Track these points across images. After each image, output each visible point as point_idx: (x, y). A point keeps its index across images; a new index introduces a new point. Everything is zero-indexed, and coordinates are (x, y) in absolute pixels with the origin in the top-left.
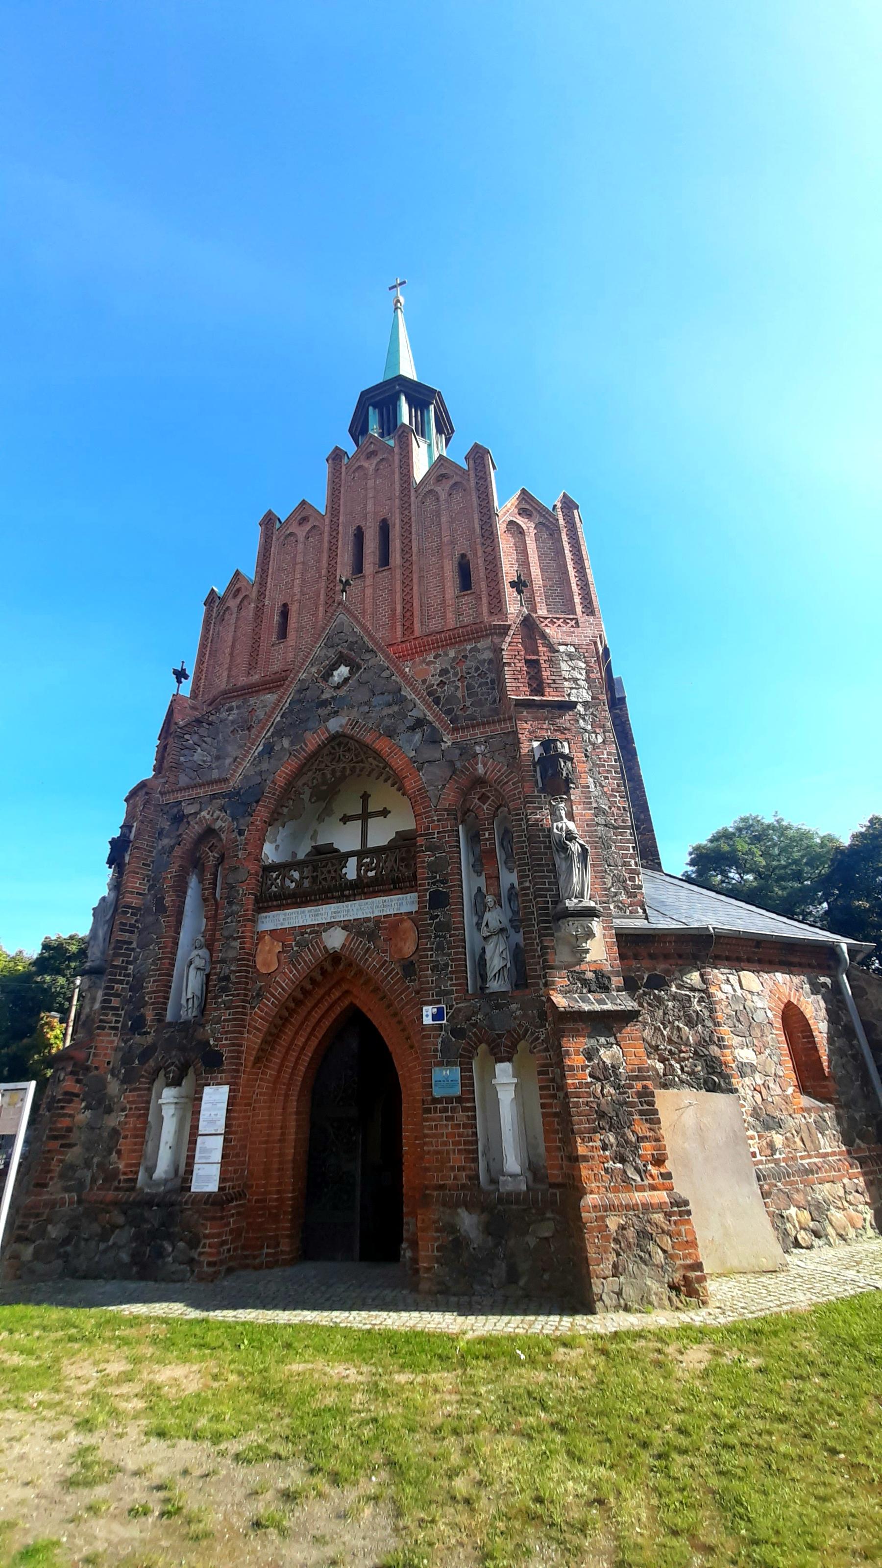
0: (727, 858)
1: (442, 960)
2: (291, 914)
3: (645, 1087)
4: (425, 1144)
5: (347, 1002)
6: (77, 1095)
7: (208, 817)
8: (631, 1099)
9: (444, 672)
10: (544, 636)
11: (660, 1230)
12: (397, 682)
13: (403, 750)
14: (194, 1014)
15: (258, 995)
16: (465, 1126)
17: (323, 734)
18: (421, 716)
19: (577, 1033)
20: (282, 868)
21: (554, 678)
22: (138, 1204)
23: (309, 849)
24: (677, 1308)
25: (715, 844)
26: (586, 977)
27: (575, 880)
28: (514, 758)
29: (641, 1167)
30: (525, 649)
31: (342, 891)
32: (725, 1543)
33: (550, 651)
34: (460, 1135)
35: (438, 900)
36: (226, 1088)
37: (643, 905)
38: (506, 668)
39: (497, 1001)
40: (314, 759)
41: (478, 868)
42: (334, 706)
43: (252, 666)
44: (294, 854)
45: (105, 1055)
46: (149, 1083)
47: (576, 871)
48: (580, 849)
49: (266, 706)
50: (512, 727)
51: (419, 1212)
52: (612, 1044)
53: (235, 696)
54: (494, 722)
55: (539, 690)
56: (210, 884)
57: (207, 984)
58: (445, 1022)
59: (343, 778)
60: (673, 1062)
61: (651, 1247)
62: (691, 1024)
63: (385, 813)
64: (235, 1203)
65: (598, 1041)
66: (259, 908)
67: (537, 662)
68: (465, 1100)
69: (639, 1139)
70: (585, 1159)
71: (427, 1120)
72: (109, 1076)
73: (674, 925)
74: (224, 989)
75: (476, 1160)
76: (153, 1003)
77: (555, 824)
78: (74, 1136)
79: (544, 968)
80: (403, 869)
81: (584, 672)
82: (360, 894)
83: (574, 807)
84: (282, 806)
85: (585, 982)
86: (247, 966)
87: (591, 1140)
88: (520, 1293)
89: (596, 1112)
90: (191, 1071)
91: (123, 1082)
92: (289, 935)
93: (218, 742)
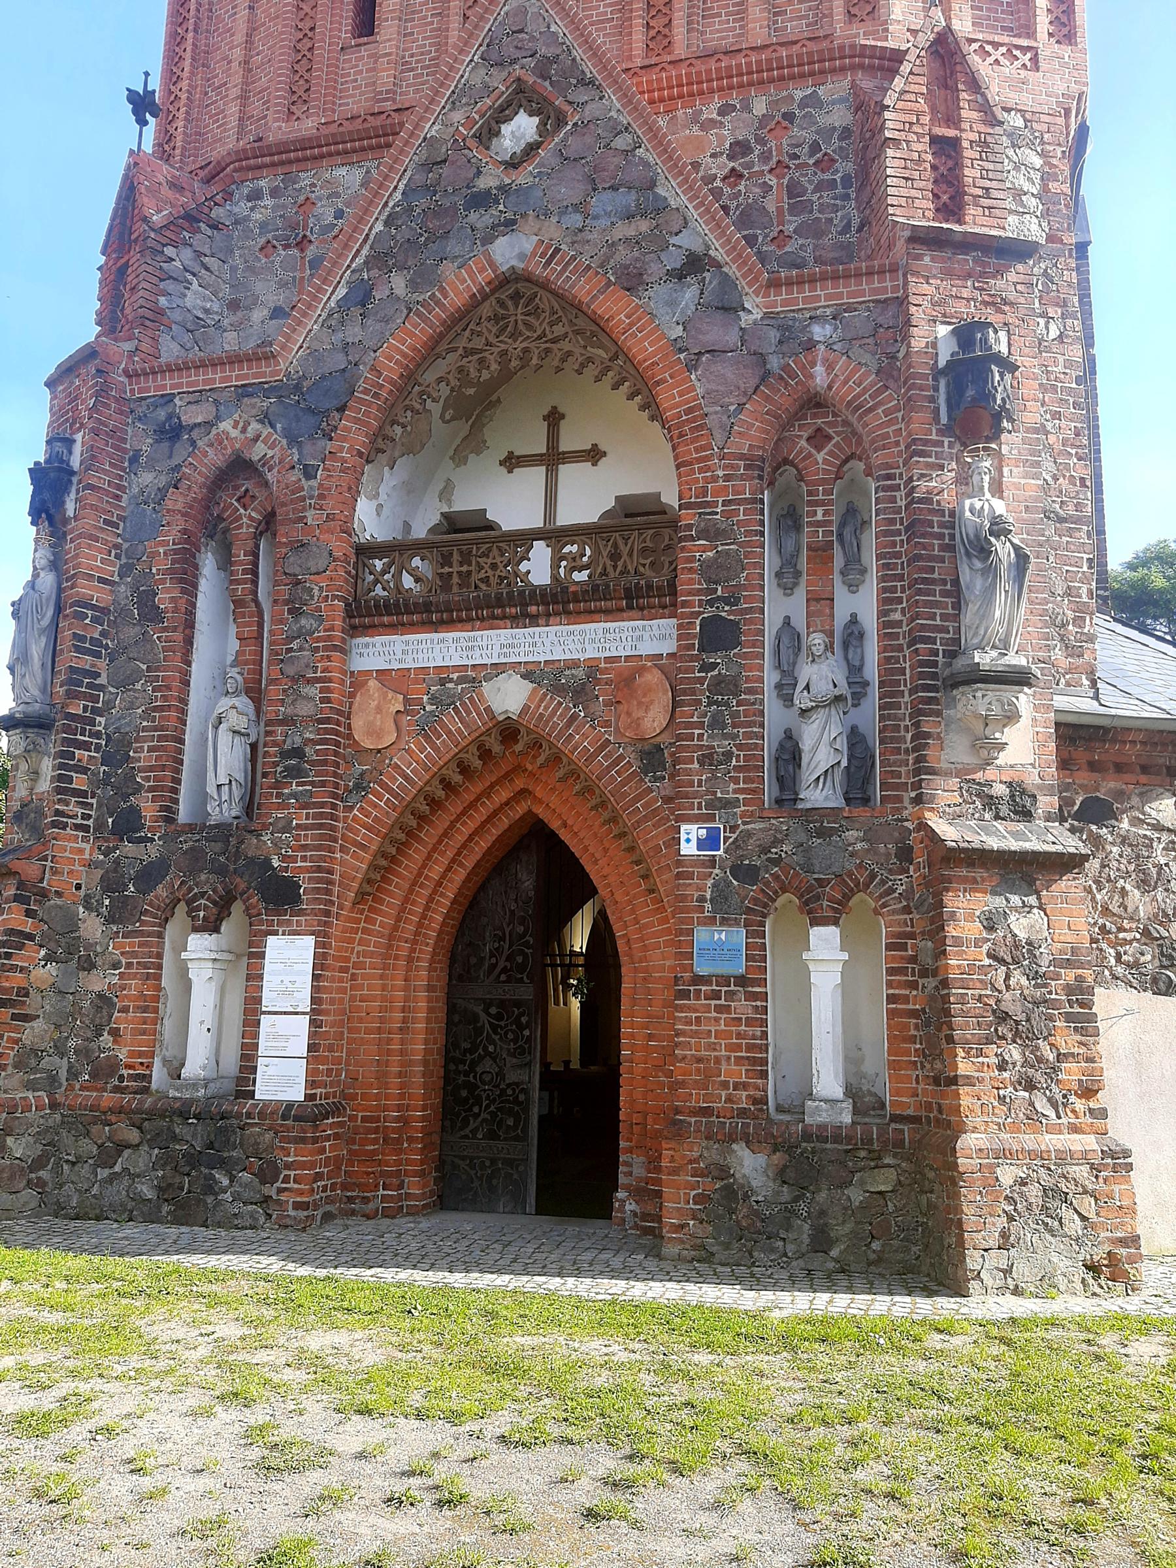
0: (1155, 604)
1: (721, 745)
2: (420, 642)
3: (1080, 979)
4: (677, 1045)
5: (520, 810)
6: (31, 937)
7: (234, 433)
8: (1053, 996)
9: (739, 149)
10: (975, 85)
11: (1080, 1189)
12: (647, 164)
13: (661, 318)
14: (234, 813)
15: (358, 787)
16: (750, 1022)
17: (482, 270)
18: (697, 247)
19: (973, 885)
20: (397, 551)
21: (987, 184)
22: (151, 1114)
23: (435, 519)
24: (1094, 1294)
25: (1142, 571)
26: (993, 792)
27: (997, 614)
28: (893, 357)
29: (1059, 1097)
30: (933, 110)
31: (524, 605)
32: (145, 1551)
33: (985, 122)
34: (739, 1035)
35: (719, 635)
36: (310, 941)
37: (1093, 672)
38: (890, 152)
39: (820, 824)
40: (458, 328)
41: (787, 580)
42: (501, 208)
43: (298, 99)
44: (407, 526)
45: (71, 872)
46: (160, 925)
47: (1000, 599)
48: (1013, 555)
49: (337, 195)
50: (895, 289)
51: (664, 1146)
52: (1031, 907)
53: (265, 166)
54: (858, 275)
55: (952, 208)
56: (245, 572)
57: (253, 759)
58: (721, 852)
59: (506, 376)
60: (1104, 946)
61: (1067, 1213)
62: (1145, 884)
63: (594, 455)
64: (330, 1121)
65: (1008, 900)
66: (354, 627)
67: (955, 143)
68: (750, 982)
69: (1060, 1057)
70: (969, 1081)
71: (681, 1009)
72: (81, 909)
73: (1148, 713)
74: (295, 773)
75: (764, 1075)
76: (151, 789)
77: (967, 503)
78: (33, 1003)
79: (917, 772)
80: (648, 572)
81: (1036, 176)
82: (557, 614)
83: (1006, 470)
84: (394, 422)
85: (990, 802)
86: (337, 733)
87: (980, 1053)
88: (831, 1265)
89: (994, 1012)
90: (237, 908)
91: (110, 920)
92: (416, 681)
93: (234, 269)
